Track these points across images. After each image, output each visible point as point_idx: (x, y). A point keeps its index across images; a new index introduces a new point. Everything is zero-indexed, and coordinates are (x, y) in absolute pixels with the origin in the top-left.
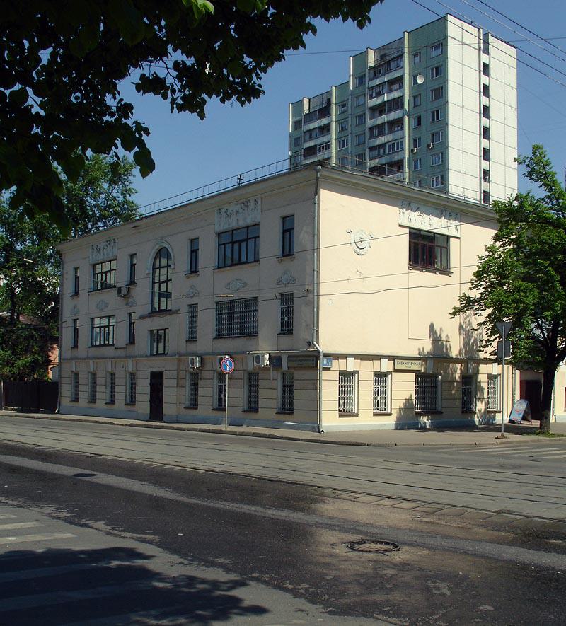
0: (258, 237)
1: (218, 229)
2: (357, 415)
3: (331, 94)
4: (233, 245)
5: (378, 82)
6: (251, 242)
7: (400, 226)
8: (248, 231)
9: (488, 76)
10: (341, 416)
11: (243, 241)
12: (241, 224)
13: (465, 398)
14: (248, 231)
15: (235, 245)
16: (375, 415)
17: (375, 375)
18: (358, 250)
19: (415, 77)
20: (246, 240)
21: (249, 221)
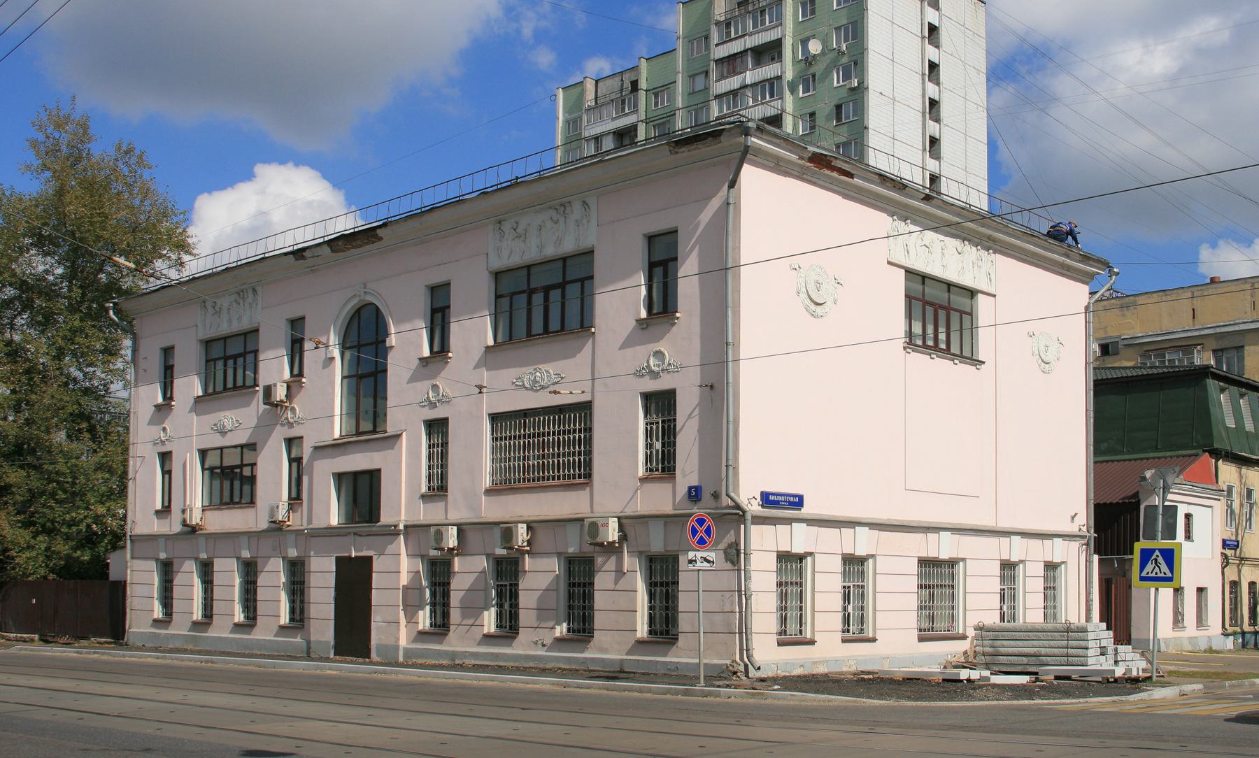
0: (592, 277)
1: (498, 263)
2: (812, 642)
3: (639, 74)
4: (377, 345)
5: (735, 47)
6: (573, 290)
7: (889, 263)
8: (529, 275)
9: (938, 47)
10: (780, 644)
11: (553, 287)
12: (550, 251)
13: (850, 609)
14: (529, 275)
15: (534, 296)
16: (844, 641)
17: (778, 557)
18: (813, 307)
19: (805, 42)
20: (562, 286)
21: (569, 246)
